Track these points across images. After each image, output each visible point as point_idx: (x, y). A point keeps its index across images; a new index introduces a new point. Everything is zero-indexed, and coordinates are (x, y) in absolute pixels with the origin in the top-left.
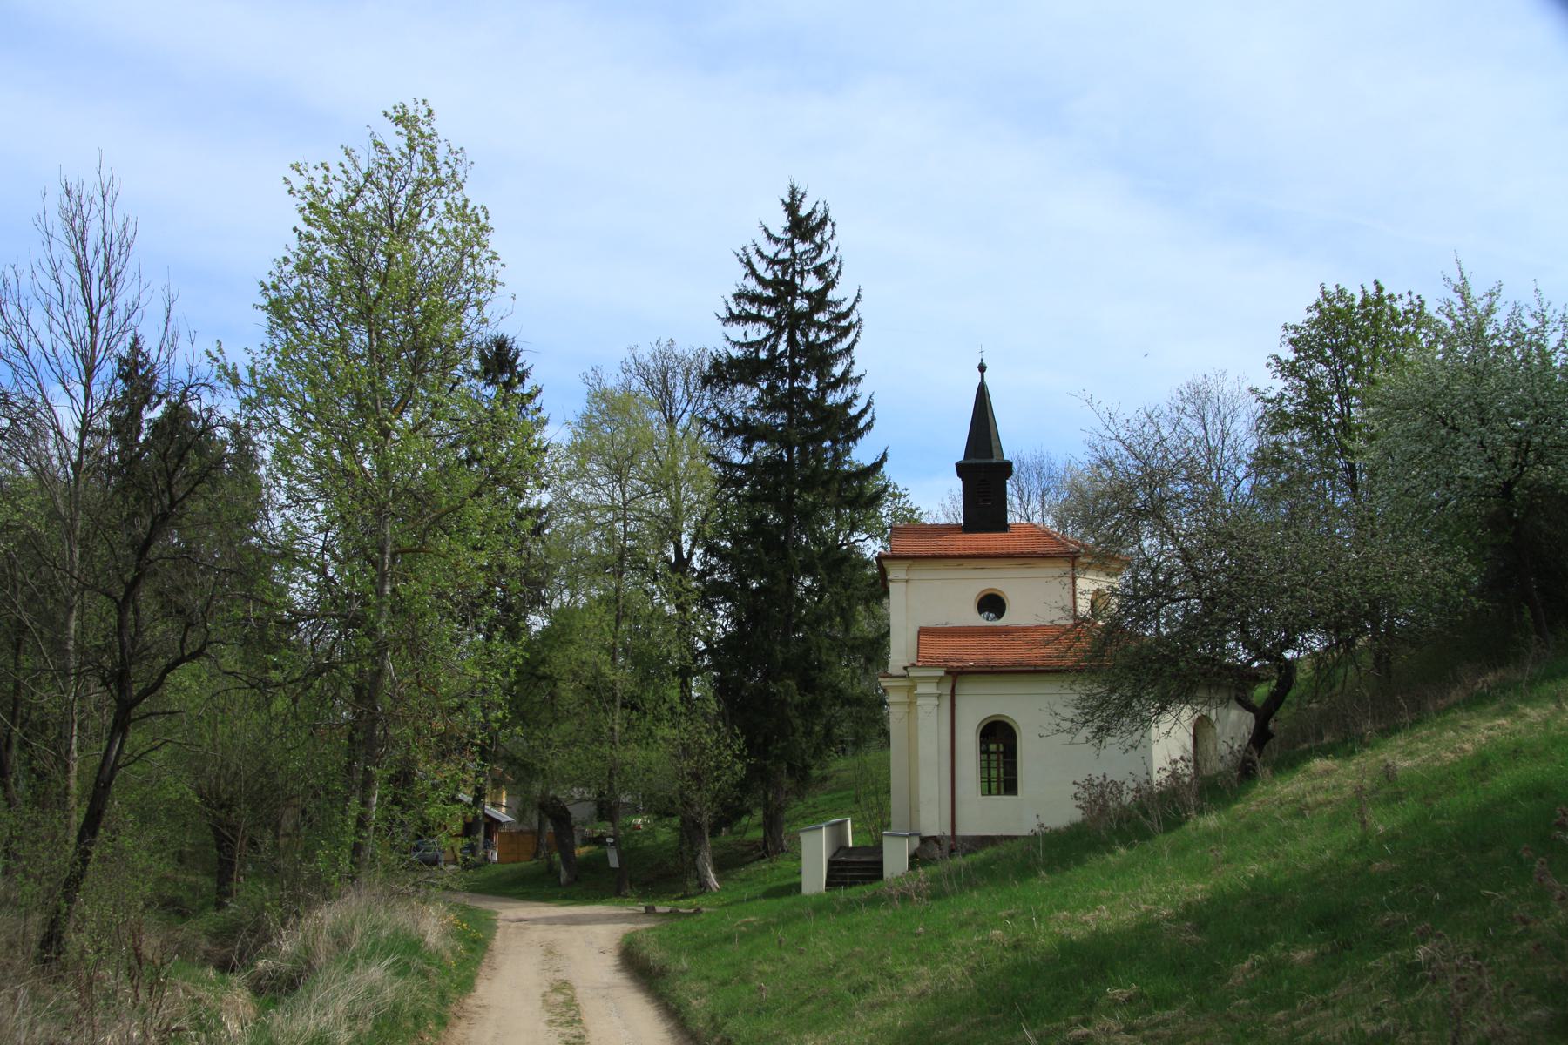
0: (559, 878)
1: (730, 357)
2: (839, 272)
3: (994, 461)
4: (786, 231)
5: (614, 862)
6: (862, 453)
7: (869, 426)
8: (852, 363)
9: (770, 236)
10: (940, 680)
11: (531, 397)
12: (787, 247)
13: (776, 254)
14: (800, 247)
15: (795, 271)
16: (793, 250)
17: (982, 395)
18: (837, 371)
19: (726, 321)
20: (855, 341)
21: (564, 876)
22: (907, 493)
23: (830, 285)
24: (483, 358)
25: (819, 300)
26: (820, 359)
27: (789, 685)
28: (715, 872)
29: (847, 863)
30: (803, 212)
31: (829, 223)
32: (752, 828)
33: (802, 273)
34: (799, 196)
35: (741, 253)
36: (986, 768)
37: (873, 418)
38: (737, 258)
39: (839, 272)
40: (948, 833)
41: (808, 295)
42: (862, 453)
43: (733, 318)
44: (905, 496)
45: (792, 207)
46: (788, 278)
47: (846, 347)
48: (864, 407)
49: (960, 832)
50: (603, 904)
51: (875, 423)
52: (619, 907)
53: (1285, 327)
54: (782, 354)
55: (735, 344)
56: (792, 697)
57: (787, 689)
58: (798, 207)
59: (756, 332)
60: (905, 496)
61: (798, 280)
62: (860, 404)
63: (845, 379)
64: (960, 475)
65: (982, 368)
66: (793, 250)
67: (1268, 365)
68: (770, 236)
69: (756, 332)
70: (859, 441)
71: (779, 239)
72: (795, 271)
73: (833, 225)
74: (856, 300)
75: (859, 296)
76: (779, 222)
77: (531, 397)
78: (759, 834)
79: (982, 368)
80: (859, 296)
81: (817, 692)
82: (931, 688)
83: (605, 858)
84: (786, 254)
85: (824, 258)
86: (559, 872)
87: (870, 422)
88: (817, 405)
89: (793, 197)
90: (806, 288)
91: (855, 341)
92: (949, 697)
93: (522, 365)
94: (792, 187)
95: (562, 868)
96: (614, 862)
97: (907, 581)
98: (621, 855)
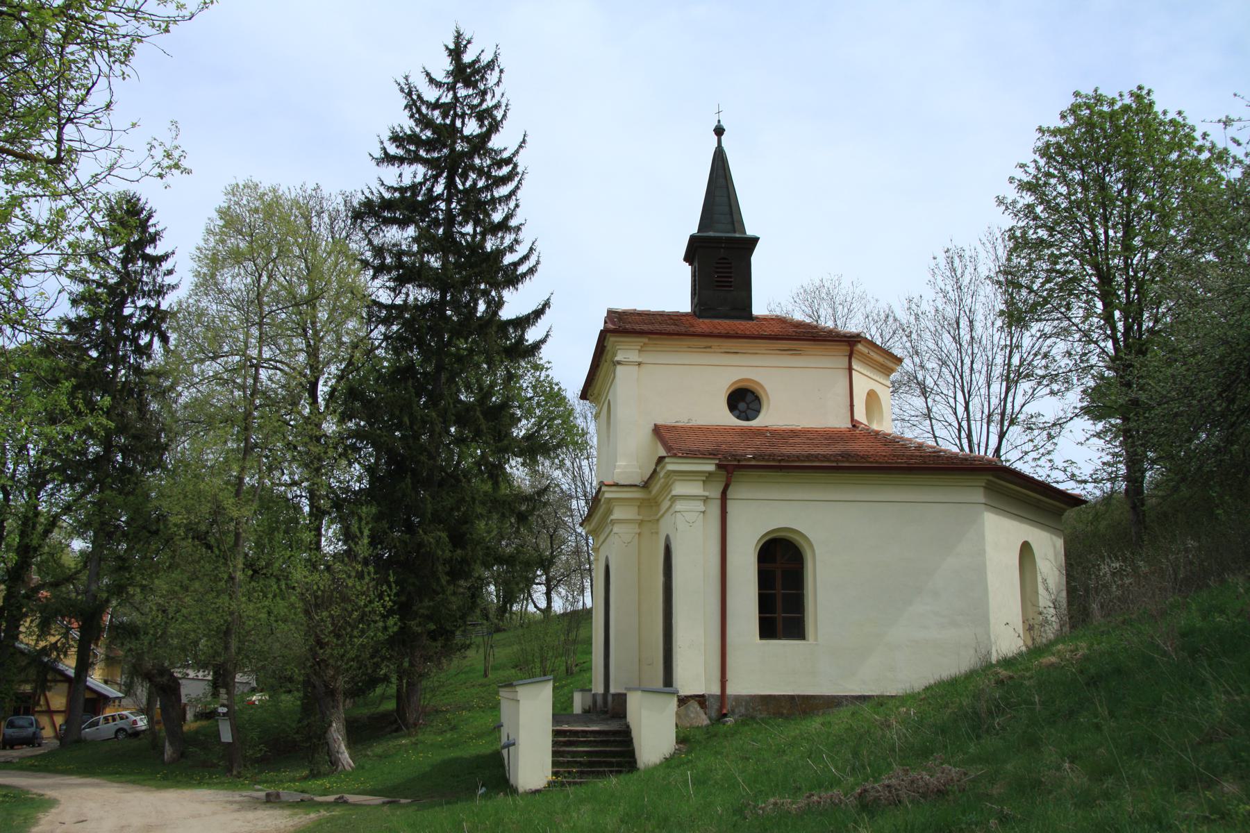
0: (163, 754)
1: (382, 197)
2: (504, 116)
3: (737, 235)
4: (449, 74)
5: (226, 736)
6: (515, 304)
7: (532, 271)
8: (517, 206)
9: (432, 81)
10: (708, 478)
11: (165, 257)
12: (448, 90)
13: (438, 100)
14: (462, 92)
15: (456, 115)
16: (455, 94)
17: (720, 165)
18: (497, 217)
19: (379, 162)
20: (517, 188)
21: (169, 751)
22: (549, 366)
23: (495, 127)
24: (111, 213)
25: (479, 144)
26: (476, 206)
27: (440, 537)
28: (349, 746)
29: (570, 731)
30: (467, 58)
31: (497, 70)
32: (384, 699)
33: (463, 116)
34: (464, 43)
35: (402, 82)
36: (765, 603)
37: (538, 263)
38: (398, 87)
39: (504, 116)
40: (715, 690)
41: (467, 139)
42: (515, 304)
43: (388, 159)
44: (547, 369)
45: (456, 53)
46: (448, 121)
47: (506, 193)
48: (525, 252)
49: (733, 689)
50: (209, 785)
51: (539, 267)
52: (230, 792)
53: (1040, 130)
54: (439, 197)
55: (389, 188)
56: (443, 551)
57: (436, 538)
58: (464, 52)
59: (413, 173)
60: (547, 369)
61: (458, 123)
62: (522, 250)
63: (503, 226)
64: (688, 258)
65: (719, 131)
66: (455, 94)
67: (1140, 88)
68: (432, 81)
69: (413, 173)
70: (520, 286)
71: (441, 83)
72: (456, 115)
73: (501, 71)
74: (521, 147)
75: (524, 141)
76: (442, 66)
77: (165, 257)
78: (391, 705)
79: (719, 131)
80: (524, 141)
81: (469, 548)
82: (696, 489)
83: (217, 735)
84: (447, 98)
85: (489, 103)
86: (164, 747)
87: (534, 266)
88: (476, 248)
89: (457, 44)
90: (467, 132)
91: (517, 188)
92: (718, 502)
93: (154, 225)
94: (458, 32)
95: (167, 744)
96: (226, 736)
97: (639, 364)
98: (235, 730)
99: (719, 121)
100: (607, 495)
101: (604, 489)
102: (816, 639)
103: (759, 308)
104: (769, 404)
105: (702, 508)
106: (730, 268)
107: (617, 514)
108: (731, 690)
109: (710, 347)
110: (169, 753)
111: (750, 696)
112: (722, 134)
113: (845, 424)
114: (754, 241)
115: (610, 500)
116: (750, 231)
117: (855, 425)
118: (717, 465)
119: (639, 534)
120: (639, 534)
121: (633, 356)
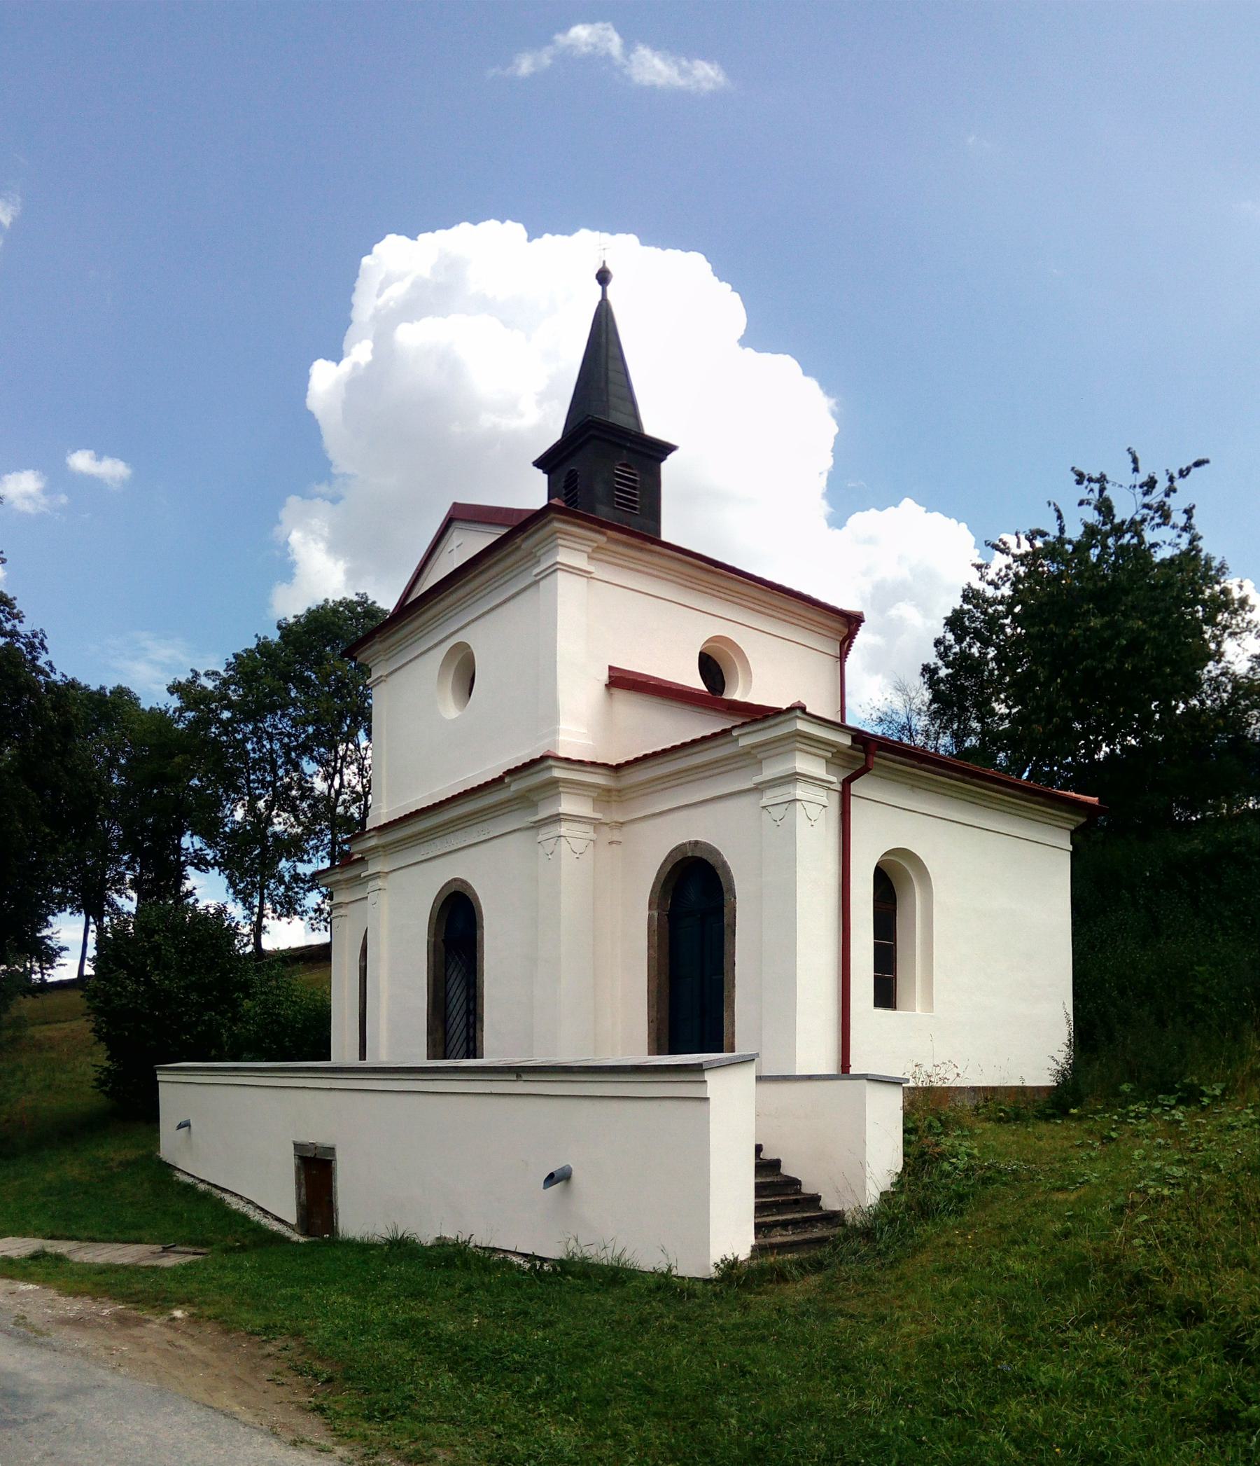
65: (603, 277)
79: (603, 277)
99: (604, 262)
116: (651, 428)
121: (580, 561)
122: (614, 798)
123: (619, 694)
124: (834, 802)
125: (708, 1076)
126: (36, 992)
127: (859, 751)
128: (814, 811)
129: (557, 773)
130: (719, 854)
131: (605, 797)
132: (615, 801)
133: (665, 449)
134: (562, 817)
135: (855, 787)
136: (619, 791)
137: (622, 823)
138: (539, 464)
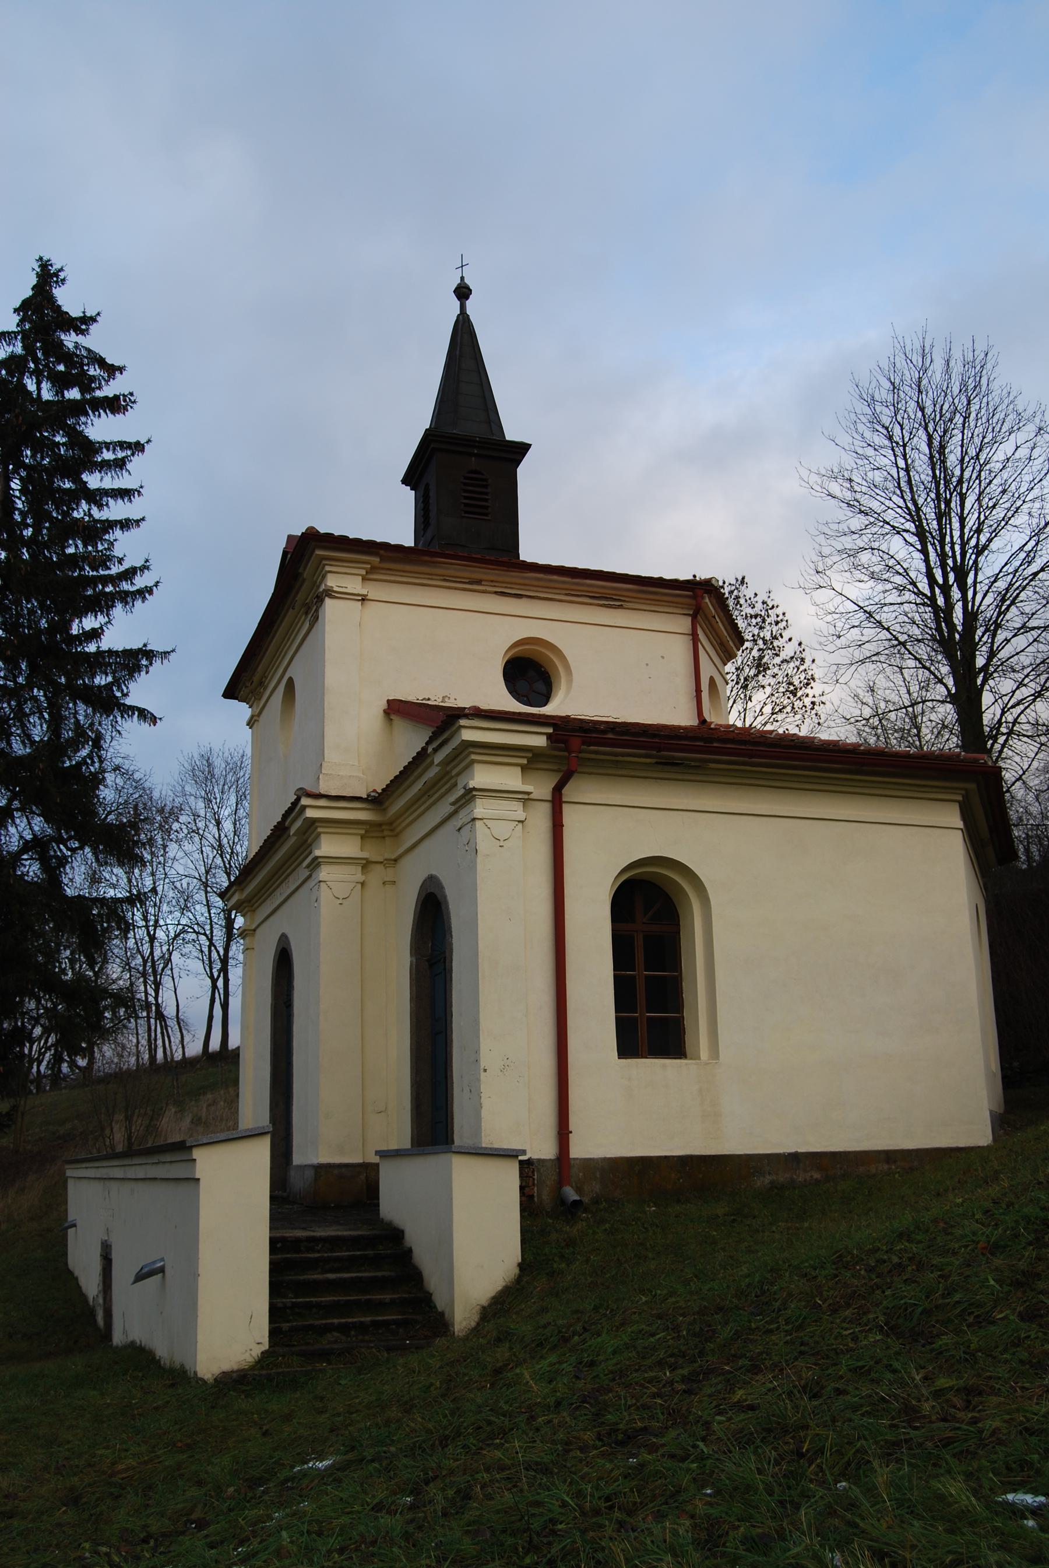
65: (463, 292)
79: (463, 292)
82: (510, 778)
99: (462, 278)
100: (310, 813)
101: (305, 801)
102: (715, 1053)
103: (528, 552)
104: (570, 681)
105: (521, 815)
106: (486, 486)
107: (327, 846)
108: (579, 1150)
109: (479, 582)
110: (943, 1380)
111: (605, 1159)
112: (467, 298)
113: (564, 800)
114: (522, 449)
115: (313, 822)
116: (512, 434)
117: (703, 722)
118: (549, 736)
119: (363, 884)
120: (363, 884)
121: (353, 584)
122: (386, 833)
123: (398, 722)
124: (540, 818)
125: (197, 1153)
126: (56, 1050)
127: (560, 750)
128: (502, 829)
129: (468, 735)
130: (443, 888)
131: (370, 832)
132: (389, 836)
133: (522, 449)
134: (320, 860)
135: (569, 792)
136: (391, 824)
137: (395, 860)
138: (230, 693)
